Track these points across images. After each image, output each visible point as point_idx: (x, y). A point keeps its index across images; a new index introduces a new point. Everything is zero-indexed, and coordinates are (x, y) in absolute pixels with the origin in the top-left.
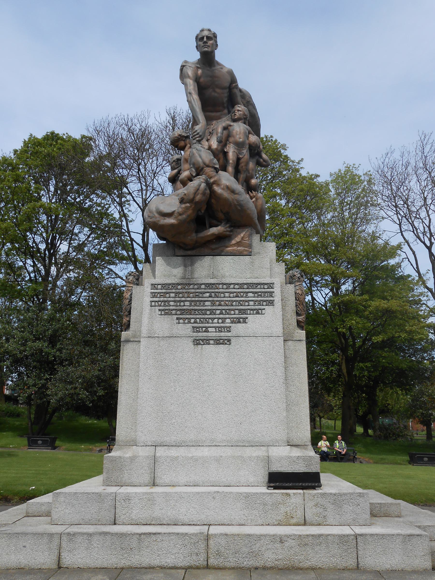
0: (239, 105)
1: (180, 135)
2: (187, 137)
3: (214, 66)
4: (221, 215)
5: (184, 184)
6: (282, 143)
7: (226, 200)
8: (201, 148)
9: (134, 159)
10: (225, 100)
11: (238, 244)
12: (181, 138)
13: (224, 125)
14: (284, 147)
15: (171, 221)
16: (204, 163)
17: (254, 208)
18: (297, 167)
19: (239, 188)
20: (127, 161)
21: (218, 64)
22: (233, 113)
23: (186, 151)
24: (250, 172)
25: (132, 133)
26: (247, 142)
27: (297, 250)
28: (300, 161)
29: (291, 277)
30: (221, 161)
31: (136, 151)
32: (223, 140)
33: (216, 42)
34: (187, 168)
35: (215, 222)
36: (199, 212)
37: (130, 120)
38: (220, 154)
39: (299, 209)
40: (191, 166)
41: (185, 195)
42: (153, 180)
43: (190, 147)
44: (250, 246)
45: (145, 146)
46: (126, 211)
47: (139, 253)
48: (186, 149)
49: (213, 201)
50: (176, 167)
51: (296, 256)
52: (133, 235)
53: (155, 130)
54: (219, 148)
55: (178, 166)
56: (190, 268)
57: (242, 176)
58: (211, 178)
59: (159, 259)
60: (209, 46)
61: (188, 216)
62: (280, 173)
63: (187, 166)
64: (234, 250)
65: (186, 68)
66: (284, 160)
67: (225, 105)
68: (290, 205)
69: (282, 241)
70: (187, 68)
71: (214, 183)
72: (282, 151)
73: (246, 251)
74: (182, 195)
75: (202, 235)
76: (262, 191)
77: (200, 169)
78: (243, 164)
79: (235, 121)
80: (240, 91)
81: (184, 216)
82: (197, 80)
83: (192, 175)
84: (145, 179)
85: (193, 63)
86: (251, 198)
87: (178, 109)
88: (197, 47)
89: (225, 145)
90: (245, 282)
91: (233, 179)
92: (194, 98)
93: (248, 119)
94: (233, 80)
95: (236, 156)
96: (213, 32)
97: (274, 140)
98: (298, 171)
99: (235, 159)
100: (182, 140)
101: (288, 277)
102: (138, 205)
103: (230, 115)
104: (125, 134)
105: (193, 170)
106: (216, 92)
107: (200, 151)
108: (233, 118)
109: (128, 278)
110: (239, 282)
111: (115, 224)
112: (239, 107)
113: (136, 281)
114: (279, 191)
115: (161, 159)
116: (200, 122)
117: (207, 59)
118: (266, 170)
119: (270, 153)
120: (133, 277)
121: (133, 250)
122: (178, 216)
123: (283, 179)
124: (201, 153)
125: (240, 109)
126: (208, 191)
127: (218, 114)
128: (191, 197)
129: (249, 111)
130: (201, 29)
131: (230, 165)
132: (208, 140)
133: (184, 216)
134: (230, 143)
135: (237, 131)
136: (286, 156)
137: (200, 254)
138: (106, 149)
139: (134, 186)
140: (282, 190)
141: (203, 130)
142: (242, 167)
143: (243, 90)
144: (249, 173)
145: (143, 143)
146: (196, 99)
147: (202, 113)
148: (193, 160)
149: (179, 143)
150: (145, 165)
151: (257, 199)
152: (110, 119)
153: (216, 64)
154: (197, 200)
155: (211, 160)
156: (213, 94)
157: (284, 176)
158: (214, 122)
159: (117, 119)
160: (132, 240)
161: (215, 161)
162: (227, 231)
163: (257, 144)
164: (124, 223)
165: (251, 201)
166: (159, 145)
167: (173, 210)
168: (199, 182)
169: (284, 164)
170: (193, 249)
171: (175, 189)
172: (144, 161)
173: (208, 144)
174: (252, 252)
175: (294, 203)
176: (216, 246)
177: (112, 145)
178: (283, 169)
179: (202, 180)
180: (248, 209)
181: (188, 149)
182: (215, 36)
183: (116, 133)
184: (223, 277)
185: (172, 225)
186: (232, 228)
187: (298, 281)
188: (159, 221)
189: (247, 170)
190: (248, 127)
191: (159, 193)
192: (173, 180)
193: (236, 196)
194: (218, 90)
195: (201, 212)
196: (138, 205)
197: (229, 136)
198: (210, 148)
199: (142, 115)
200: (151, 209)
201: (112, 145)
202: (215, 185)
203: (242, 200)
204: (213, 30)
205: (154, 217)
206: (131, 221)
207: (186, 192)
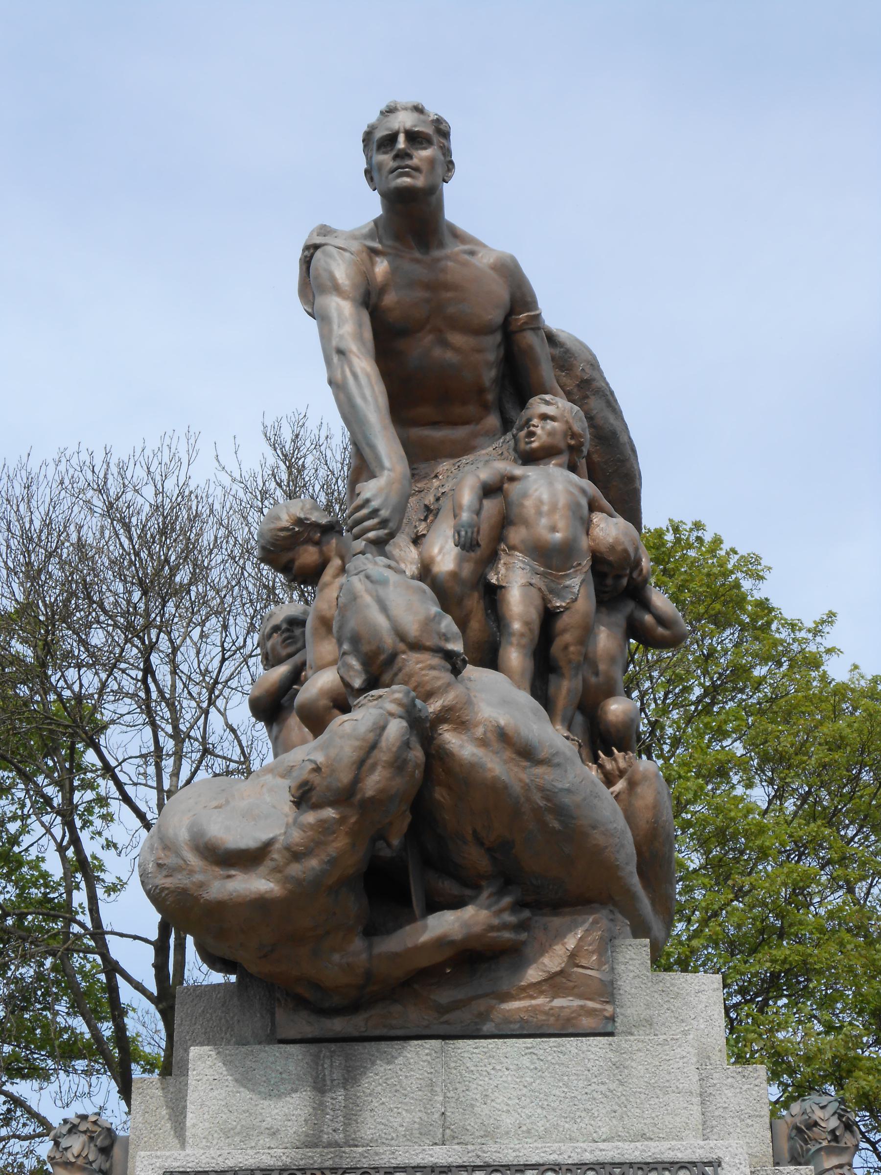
0: (547, 397)
1: (299, 521)
2: (331, 529)
3: (441, 245)
4: (475, 858)
5: (316, 722)
6: (743, 551)
7: (496, 790)
8: (388, 573)
9: (129, 627)
10: (489, 375)
11: (555, 983)
12: (304, 532)
13: (485, 474)
14: (753, 567)
15: (258, 884)
16: (401, 636)
17: (621, 823)
18: (812, 648)
19: (552, 736)
20: (97, 637)
21: (457, 235)
22: (521, 429)
23: (327, 585)
24: (602, 667)
25: (122, 520)
26: (584, 543)
27: (827, 1003)
28: (823, 622)
29: (799, 1130)
30: (475, 624)
31: (137, 595)
32: (483, 539)
33: (446, 151)
34: (330, 658)
35: (449, 887)
36: (381, 844)
37: (114, 469)
38: (472, 597)
39: (830, 824)
40: (346, 647)
41: (317, 769)
42: (207, 712)
43: (343, 570)
44: (608, 991)
45: (173, 575)
46: (91, 847)
47: (144, 1023)
48: (327, 576)
49: (440, 794)
50: (284, 652)
51: (829, 1028)
52: (117, 948)
53: (217, 506)
54: (467, 570)
55: (290, 649)
56: (340, 1095)
57: (565, 688)
58: (428, 696)
59: (200, 1057)
60: (417, 169)
61: (333, 862)
62: (740, 672)
63: (327, 648)
64: (535, 1010)
65: (326, 254)
66: (754, 620)
67: (490, 397)
68: (790, 805)
69: (761, 966)
70: (328, 255)
71: (446, 716)
72: (747, 584)
73: (592, 1012)
74: (304, 773)
75: (395, 943)
76: (666, 748)
77: (382, 657)
78: (568, 637)
79: (530, 458)
80: (551, 339)
81: (314, 863)
82: (370, 300)
83: (347, 685)
84: (171, 705)
85: (353, 236)
86: (609, 781)
87: (311, 424)
88: (368, 172)
89: (492, 558)
90: (588, 1157)
91: (525, 698)
92: (359, 371)
93: (585, 450)
94: (521, 299)
95: (538, 602)
96: (433, 117)
97: (708, 537)
98: (814, 662)
99: (534, 615)
100: (309, 541)
101: (783, 1129)
102: (141, 816)
103: (509, 436)
104: (93, 527)
105: (354, 662)
106: (451, 347)
107: (384, 582)
108: (522, 446)
109: (64, 1143)
110: (560, 1159)
111: (46, 899)
112: (547, 403)
113: (101, 1158)
114: (739, 749)
115: (238, 626)
116: (382, 467)
117: (413, 216)
118: (680, 660)
119: (694, 593)
120: (83, 1138)
121: (118, 1012)
122: (287, 864)
123: (754, 701)
124: (387, 593)
125: (550, 410)
126: (417, 754)
127: (460, 433)
128: (345, 777)
129: (590, 418)
130: (383, 107)
131: (514, 640)
132: (417, 540)
133: (314, 863)
134: (512, 548)
135: (541, 502)
136: (764, 606)
137: (384, 1032)
138: (15, 586)
139: (125, 740)
140: (752, 745)
141: (394, 499)
142: (566, 647)
143: (562, 337)
144: (597, 674)
145: (167, 561)
146: (368, 375)
147: (392, 430)
148: (352, 624)
149: (296, 552)
150: (175, 650)
151: (632, 785)
152: (34, 465)
153: (448, 239)
154: (369, 793)
155: (429, 622)
156: (438, 352)
157: (758, 684)
158: (444, 466)
159: (62, 467)
160: (112, 968)
161: (448, 623)
162: (505, 927)
163: (625, 551)
164: (80, 897)
165: (607, 794)
166: (231, 569)
167: (265, 836)
168: (377, 716)
169: (756, 638)
170: (353, 1007)
171: (280, 746)
172: (169, 633)
173: (420, 554)
174: (618, 1020)
175: (804, 798)
176: (456, 994)
177: (40, 571)
178: (755, 655)
179: (392, 707)
180: (594, 827)
181: (336, 576)
182: (442, 131)
183: (58, 517)
184: (490, 1134)
185: (261, 905)
186: (526, 914)
187: (830, 1151)
188: (201, 885)
189: (589, 661)
190: (586, 483)
191: (233, 766)
192: (271, 708)
193: (539, 770)
194: (457, 339)
195: (389, 845)
196: (141, 816)
197: (506, 521)
198: (425, 573)
199: (166, 450)
200: (171, 832)
201: (40, 571)
202: (445, 727)
203: (568, 791)
204: (433, 109)
205: (183, 868)
206: (112, 889)
207: (320, 758)
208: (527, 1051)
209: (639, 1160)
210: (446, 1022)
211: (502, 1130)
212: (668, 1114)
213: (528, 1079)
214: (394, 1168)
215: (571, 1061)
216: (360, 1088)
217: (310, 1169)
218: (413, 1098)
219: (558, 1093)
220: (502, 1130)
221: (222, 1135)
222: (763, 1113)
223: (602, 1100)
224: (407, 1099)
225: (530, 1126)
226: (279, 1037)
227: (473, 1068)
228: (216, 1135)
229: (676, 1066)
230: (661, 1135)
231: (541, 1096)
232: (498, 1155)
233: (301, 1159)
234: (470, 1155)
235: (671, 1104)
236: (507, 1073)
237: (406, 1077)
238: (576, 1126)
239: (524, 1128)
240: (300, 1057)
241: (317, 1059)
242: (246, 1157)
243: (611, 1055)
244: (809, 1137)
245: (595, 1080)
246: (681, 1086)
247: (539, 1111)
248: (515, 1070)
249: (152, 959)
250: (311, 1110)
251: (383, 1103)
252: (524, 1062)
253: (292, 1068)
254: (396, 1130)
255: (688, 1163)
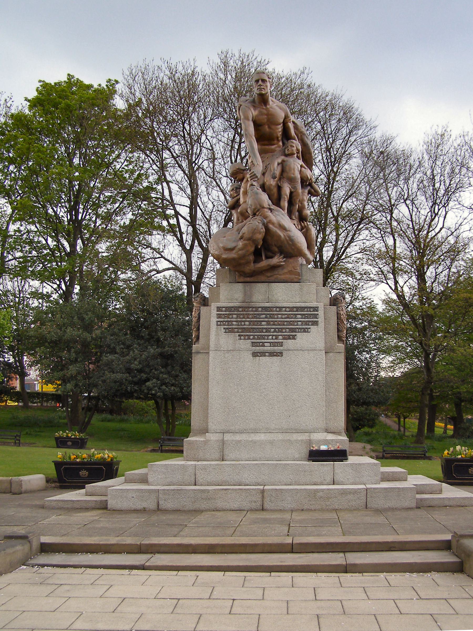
35: (270, 254)
67: (280, 139)
73: (296, 278)
249: (188, 211)
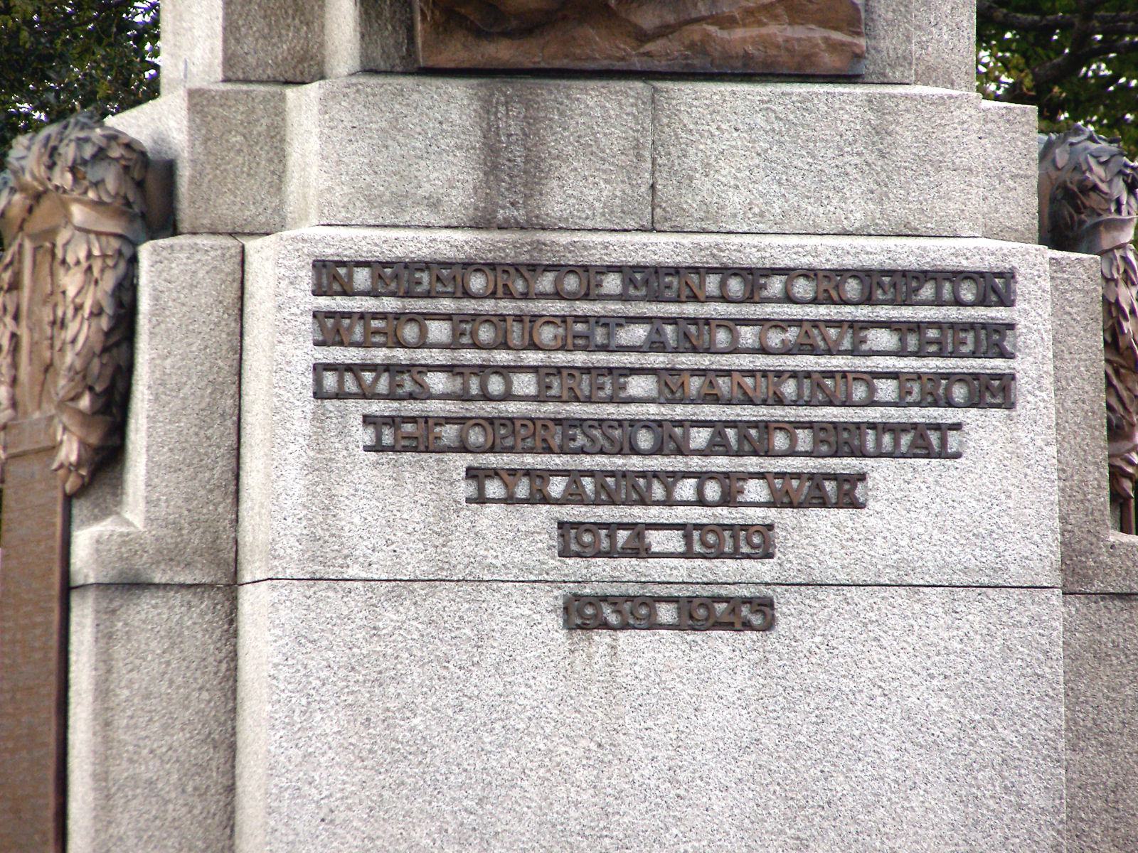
64: (765, 42)
73: (834, 47)
110: (816, 263)
208: (762, 106)
209: (915, 266)
210: (648, 54)
211: (729, 210)
212: (940, 198)
213: (761, 144)
214: (608, 266)
215: (818, 120)
216: (545, 147)
217: (501, 264)
218: (613, 164)
219: (800, 165)
220: (729, 210)
221: (365, 204)
222: (1029, 173)
223: (856, 176)
224: (607, 166)
225: (764, 208)
226: (422, 63)
227: (691, 127)
228: (358, 203)
229: (954, 134)
230: (929, 225)
231: (779, 167)
232: (738, 254)
233: (490, 251)
234: (703, 253)
235: (944, 185)
236: (735, 134)
237: (605, 134)
238: (821, 210)
239: (756, 210)
240: (465, 102)
241: (488, 107)
242: (419, 245)
243: (870, 115)
244: (1083, 203)
245: (849, 149)
246: (957, 161)
247: (775, 187)
248: (746, 132)
250: (481, 175)
251: (576, 169)
252: (759, 121)
253: (454, 116)
254: (592, 207)
255: (974, 272)
